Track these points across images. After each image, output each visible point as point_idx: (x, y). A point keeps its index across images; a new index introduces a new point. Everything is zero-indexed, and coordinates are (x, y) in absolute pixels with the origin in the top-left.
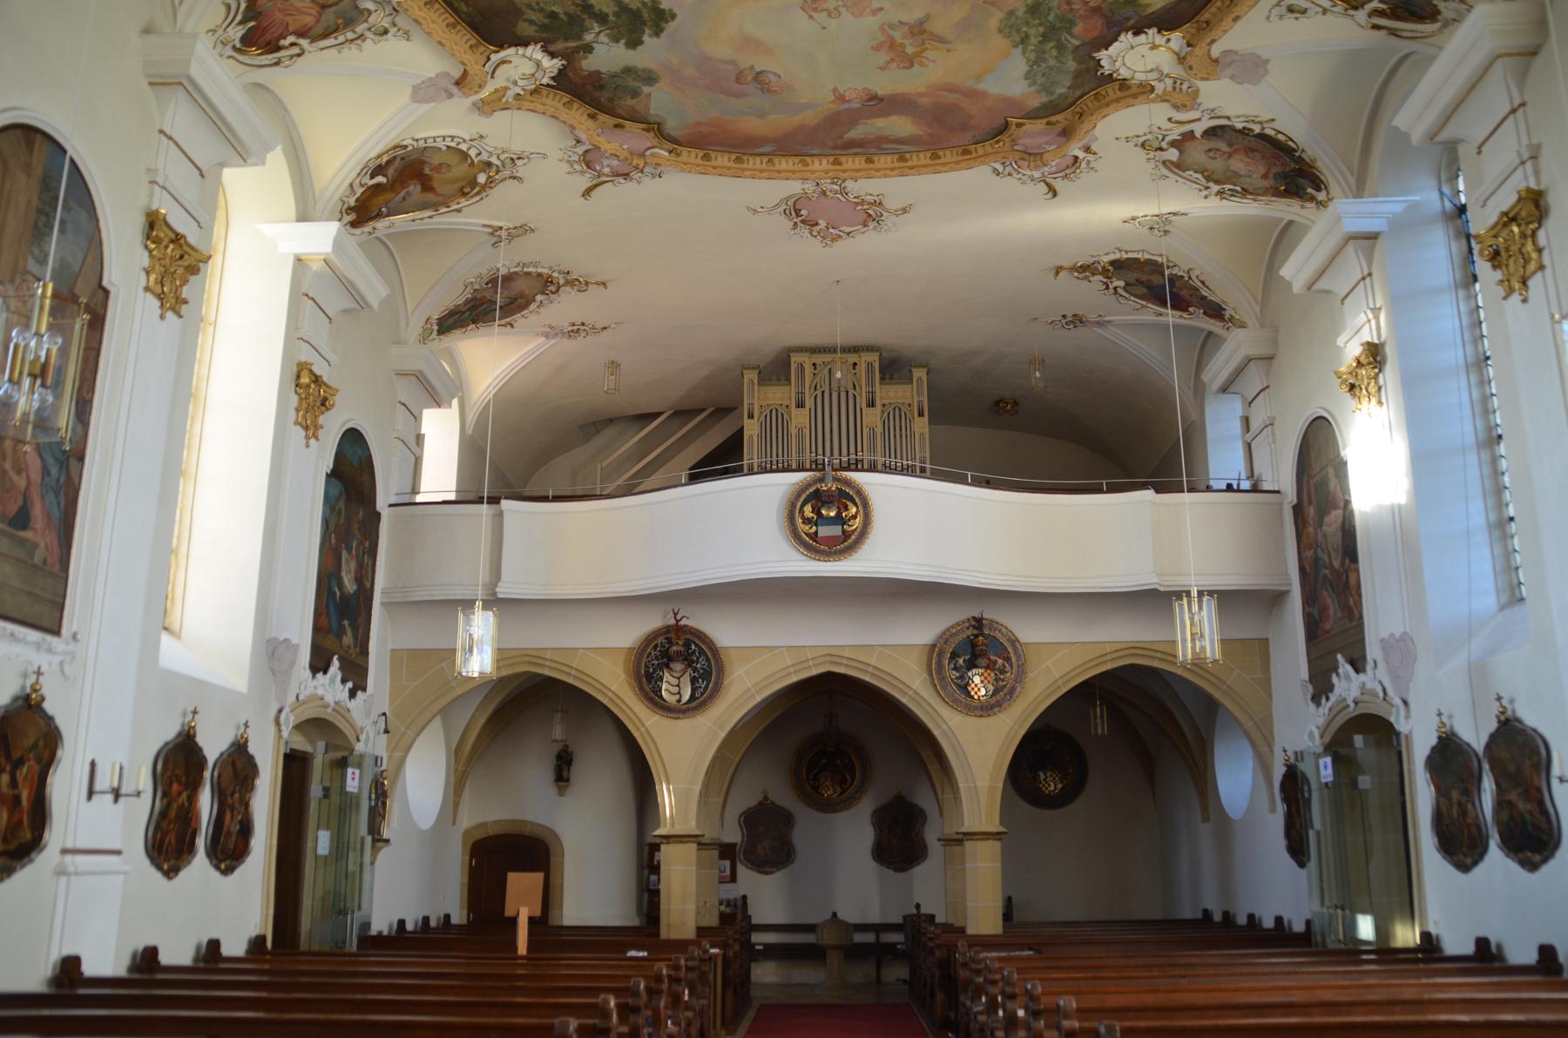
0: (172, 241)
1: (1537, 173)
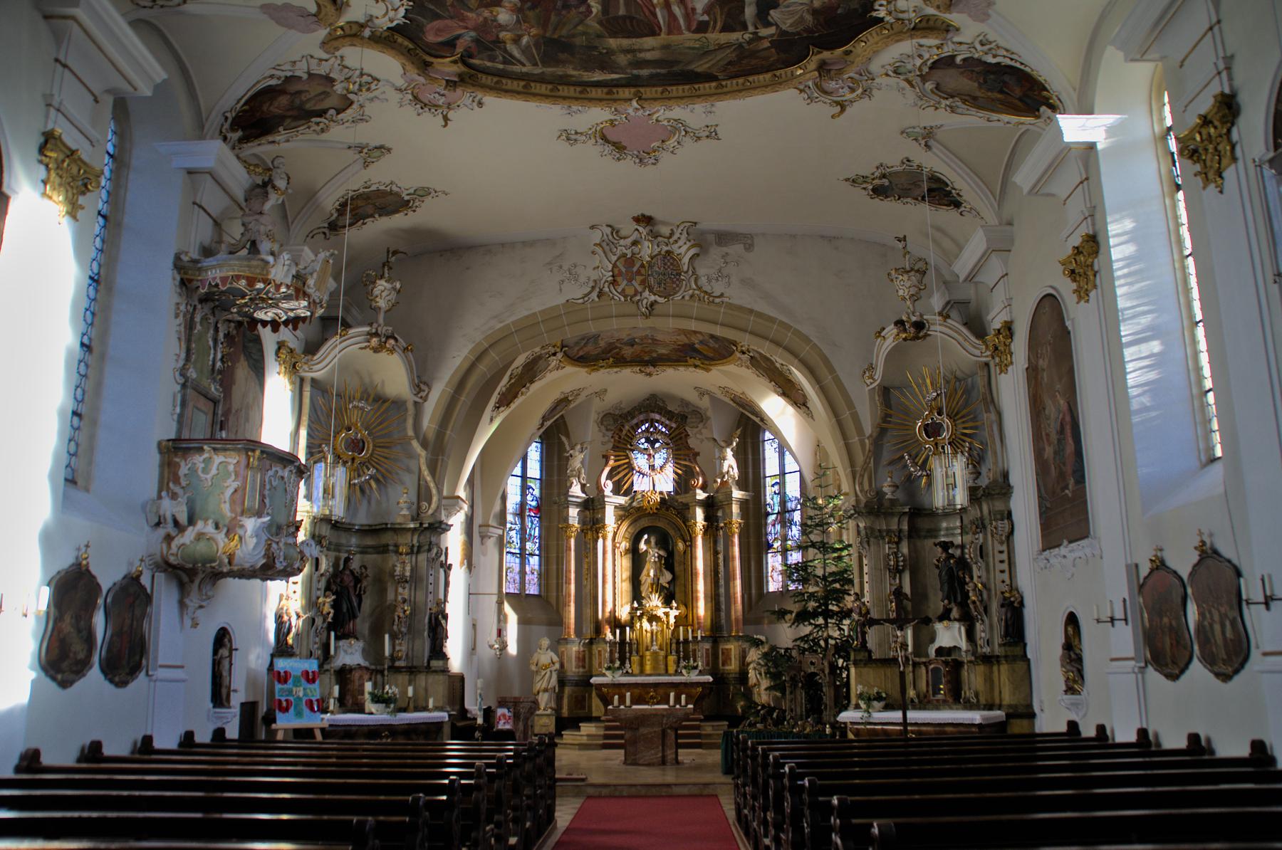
0: (68, 156)
1: (1230, 79)
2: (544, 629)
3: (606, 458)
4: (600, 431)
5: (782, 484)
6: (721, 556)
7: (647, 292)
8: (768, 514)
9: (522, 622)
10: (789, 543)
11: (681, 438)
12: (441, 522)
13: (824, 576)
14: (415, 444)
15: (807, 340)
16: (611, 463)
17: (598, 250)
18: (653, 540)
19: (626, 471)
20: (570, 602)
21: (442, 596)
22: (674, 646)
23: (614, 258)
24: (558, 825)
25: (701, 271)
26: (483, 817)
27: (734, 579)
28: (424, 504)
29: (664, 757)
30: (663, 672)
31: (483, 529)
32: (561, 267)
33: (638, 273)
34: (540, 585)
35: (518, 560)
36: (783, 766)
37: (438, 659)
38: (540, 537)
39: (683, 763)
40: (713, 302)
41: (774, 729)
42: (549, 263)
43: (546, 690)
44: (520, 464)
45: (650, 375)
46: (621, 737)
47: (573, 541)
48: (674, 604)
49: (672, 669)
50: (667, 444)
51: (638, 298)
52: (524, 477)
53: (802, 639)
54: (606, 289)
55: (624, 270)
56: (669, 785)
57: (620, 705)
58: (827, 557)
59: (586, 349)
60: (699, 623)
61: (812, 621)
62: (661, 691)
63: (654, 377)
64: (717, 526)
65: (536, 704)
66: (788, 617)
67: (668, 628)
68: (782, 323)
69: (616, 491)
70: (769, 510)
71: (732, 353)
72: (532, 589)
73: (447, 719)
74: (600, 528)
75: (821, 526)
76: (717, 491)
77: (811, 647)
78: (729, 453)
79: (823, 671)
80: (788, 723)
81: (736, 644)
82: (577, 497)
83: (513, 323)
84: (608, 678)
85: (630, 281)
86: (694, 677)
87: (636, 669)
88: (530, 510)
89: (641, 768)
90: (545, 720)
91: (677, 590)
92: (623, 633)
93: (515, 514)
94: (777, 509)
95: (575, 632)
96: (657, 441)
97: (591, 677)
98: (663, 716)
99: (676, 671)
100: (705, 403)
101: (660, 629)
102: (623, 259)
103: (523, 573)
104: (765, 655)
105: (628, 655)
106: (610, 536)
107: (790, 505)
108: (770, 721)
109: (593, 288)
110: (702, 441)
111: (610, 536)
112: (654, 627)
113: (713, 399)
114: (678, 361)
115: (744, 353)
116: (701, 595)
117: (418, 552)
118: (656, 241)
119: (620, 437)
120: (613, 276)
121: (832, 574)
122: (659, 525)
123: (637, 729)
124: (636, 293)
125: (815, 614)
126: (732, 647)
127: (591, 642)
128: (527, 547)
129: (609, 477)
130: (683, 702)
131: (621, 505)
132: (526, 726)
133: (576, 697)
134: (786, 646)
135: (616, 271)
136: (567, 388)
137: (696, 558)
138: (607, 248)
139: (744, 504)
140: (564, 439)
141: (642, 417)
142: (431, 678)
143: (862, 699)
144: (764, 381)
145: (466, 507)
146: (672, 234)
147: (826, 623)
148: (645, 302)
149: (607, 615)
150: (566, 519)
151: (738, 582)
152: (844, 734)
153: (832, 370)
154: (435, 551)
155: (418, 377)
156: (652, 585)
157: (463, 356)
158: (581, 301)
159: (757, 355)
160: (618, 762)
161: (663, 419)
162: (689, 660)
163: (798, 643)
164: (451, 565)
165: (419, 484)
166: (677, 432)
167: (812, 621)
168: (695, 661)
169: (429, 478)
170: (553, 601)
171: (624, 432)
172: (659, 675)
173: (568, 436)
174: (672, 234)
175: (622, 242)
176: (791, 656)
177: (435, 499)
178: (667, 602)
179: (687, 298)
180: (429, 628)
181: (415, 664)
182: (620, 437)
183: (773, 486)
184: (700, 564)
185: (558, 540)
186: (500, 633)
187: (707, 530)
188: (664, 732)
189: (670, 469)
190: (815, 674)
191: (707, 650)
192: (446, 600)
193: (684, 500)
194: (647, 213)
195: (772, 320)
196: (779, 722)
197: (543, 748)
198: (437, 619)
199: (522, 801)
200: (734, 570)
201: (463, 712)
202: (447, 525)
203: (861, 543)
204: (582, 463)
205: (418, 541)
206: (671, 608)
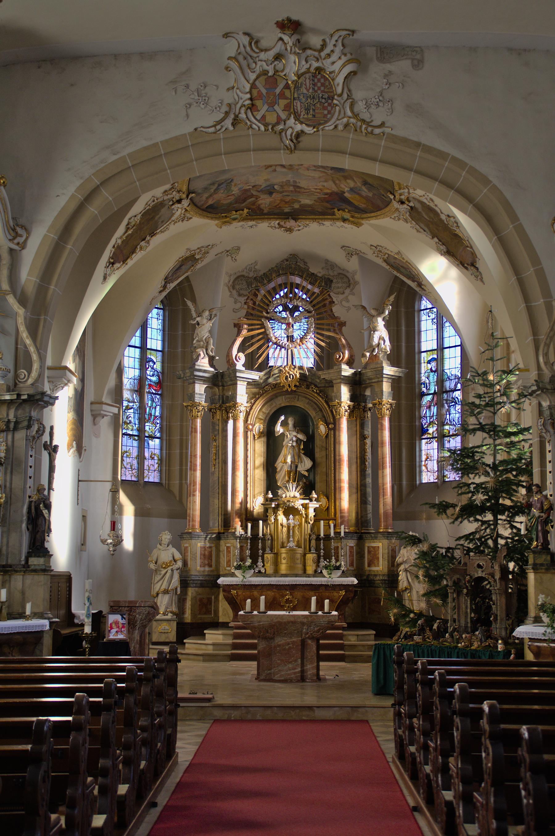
2: (164, 522)
3: (238, 327)
4: (231, 296)
5: (440, 360)
6: (368, 441)
7: (292, 120)
8: (423, 395)
9: (139, 514)
10: (447, 427)
11: (324, 306)
12: (43, 394)
13: (494, 463)
14: (11, 300)
15: (485, 181)
16: (244, 332)
17: (233, 65)
18: (291, 422)
19: (261, 342)
20: (195, 491)
21: (44, 481)
22: (313, 542)
23: (252, 77)
24: (179, 760)
25: (358, 95)
26: (83, 766)
27: (383, 468)
28: (23, 372)
29: (303, 671)
30: (300, 572)
31: (95, 407)
32: (187, 86)
33: (282, 95)
34: (161, 472)
35: (135, 444)
36: (432, 672)
37: (39, 556)
38: (161, 417)
39: (325, 680)
40: (372, 133)
41: (435, 642)
42: (173, 82)
43: (166, 592)
44: (138, 334)
45: (290, 230)
46: (253, 646)
47: (199, 422)
48: (314, 495)
49: (310, 569)
50: (309, 312)
51: (281, 127)
52: (143, 348)
53: (467, 537)
54: (243, 116)
55: (264, 91)
56: (310, 708)
57: (252, 610)
58: (498, 441)
59: (217, 197)
60: (342, 517)
61: (478, 517)
62: (298, 594)
63: (295, 233)
64: (365, 407)
65: (155, 608)
66: (450, 511)
67: (306, 521)
68: (455, 160)
69: (250, 365)
70: (424, 390)
71: (388, 203)
72: (153, 477)
73: (48, 628)
74: (230, 407)
75: (492, 406)
76: (365, 367)
77: (477, 548)
78: (380, 323)
79: (493, 575)
80: (451, 636)
81: (386, 542)
82: (205, 371)
83: (130, 155)
84: (238, 578)
85: (272, 105)
86: (336, 578)
87: (269, 568)
88: (150, 385)
89: (277, 684)
90: (164, 626)
91: (318, 479)
92: (255, 527)
93: (133, 391)
94: (433, 388)
95: (201, 526)
96: (296, 308)
97: (218, 577)
98: (303, 624)
99: (316, 571)
100: (353, 265)
101: (297, 523)
102: (263, 78)
103: (141, 458)
104: (423, 555)
105: (260, 552)
106: (242, 417)
107: (448, 385)
108: (428, 633)
109: (227, 113)
110: (348, 309)
111: (242, 417)
112: (291, 521)
113: (364, 261)
114: (323, 213)
115: (402, 203)
116: (345, 485)
117: (16, 429)
118: (304, 56)
119: (254, 303)
120: (251, 99)
121: (502, 462)
122: (300, 404)
123: (273, 638)
124: (279, 120)
125: (482, 509)
126: (380, 545)
127: (219, 537)
128: (147, 428)
129: (242, 349)
130: (326, 609)
131: (254, 381)
132: (142, 636)
133: (201, 600)
134: (448, 545)
135: (255, 92)
136: (194, 244)
137: (340, 443)
138: (244, 63)
139: (395, 381)
140: (189, 303)
141: (280, 280)
142: (30, 579)
143: (545, 612)
144: (425, 237)
145: (75, 380)
146: (324, 46)
147: (496, 520)
148: (289, 132)
149: (238, 506)
150: (192, 396)
151: (388, 471)
152: (520, 654)
153: (513, 217)
154: (35, 427)
155: (13, 219)
156: (289, 473)
157: (70, 194)
158: (212, 130)
159: (418, 206)
160: (249, 677)
161: (305, 284)
162: (330, 559)
163: (462, 542)
164: (56, 447)
165: (17, 348)
166: (320, 299)
167: (478, 517)
168: (337, 560)
169: (28, 341)
170: (176, 490)
171: (259, 298)
172: (296, 576)
173: (194, 300)
174: (324, 46)
175: (263, 56)
176: (453, 558)
177: (36, 366)
178: (306, 493)
179: (340, 127)
180: (29, 518)
181: (10, 562)
182: (254, 303)
183: (429, 362)
184: (344, 450)
185: (182, 421)
186: (114, 526)
187: (352, 411)
188: (303, 642)
189: (311, 343)
190: (481, 579)
191: (351, 547)
192: (50, 488)
193: (327, 377)
194: (294, 17)
195: (442, 155)
196: (439, 634)
197: (163, 665)
198: (37, 508)
199: (136, 735)
200: (383, 458)
201: (70, 616)
202: (51, 397)
203: (544, 425)
204: (210, 332)
205: (15, 416)
206: (311, 500)
